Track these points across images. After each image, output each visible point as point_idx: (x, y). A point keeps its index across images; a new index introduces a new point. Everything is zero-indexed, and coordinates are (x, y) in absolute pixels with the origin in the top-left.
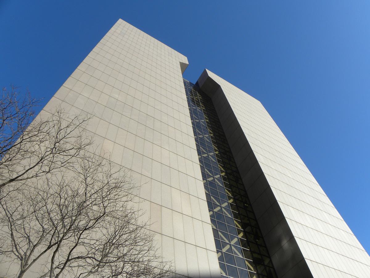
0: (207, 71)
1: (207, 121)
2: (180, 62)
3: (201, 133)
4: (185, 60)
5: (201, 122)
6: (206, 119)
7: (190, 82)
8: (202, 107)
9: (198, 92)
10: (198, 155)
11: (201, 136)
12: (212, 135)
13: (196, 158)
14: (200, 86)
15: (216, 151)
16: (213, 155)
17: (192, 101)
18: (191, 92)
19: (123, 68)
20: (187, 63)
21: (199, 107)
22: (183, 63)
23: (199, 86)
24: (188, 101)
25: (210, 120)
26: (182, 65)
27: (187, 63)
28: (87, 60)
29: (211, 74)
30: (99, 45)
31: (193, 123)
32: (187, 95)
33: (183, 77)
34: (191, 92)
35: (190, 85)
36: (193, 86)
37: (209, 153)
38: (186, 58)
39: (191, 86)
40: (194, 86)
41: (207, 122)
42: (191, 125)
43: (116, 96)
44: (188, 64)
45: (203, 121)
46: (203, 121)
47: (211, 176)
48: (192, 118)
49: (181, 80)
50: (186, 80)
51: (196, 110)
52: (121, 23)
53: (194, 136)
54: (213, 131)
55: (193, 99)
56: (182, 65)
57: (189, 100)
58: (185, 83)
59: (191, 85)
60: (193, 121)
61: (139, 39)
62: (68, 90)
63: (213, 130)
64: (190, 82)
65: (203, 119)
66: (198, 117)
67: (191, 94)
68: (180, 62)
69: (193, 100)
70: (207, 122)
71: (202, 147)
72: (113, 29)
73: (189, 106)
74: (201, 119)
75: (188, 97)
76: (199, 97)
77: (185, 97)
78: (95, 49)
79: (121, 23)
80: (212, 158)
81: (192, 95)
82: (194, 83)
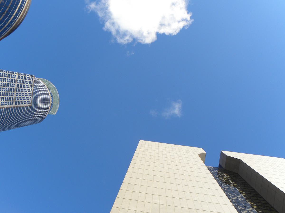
0: (223, 152)
1: (244, 194)
2: (198, 154)
3: (234, 195)
4: (201, 151)
5: (239, 198)
6: (242, 193)
7: (214, 167)
8: (227, 176)
9: (224, 172)
10: (229, 199)
11: (235, 198)
12: (255, 207)
13: (228, 201)
14: (224, 166)
15: (253, 205)
16: (252, 210)
17: (222, 183)
18: (218, 175)
19: (142, 186)
20: (204, 152)
21: (231, 185)
22: (201, 154)
23: (223, 168)
24: (219, 184)
25: (257, 206)
26: (201, 155)
27: (204, 152)
28: (126, 180)
29: (228, 154)
30: (131, 165)
31: (232, 202)
32: (215, 179)
33: (206, 165)
34: (218, 175)
35: (215, 169)
36: (218, 169)
37: (248, 209)
38: (202, 149)
39: (216, 170)
40: (218, 169)
41: (245, 196)
42: (231, 204)
43: (158, 201)
44: (205, 153)
45: (240, 196)
46: (241, 197)
47: (245, 210)
48: (229, 198)
49: (206, 167)
50: (209, 167)
51: (229, 188)
52: (141, 141)
53: (229, 199)
54: (243, 191)
55: (222, 180)
56: (201, 155)
57: (219, 182)
58: (209, 169)
59: (216, 169)
60: (231, 200)
61: (163, 148)
62: (118, 209)
63: (253, 202)
64: (214, 167)
65: (240, 195)
66: (234, 194)
67: (218, 176)
68: (198, 154)
69: (223, 181)
70: (245, 196)
71: (239, 206)
72: (137, 149)
73: (222, 188)
74: (238, 195)
75: (217, 180)
76: (227, 177)
77: (214, 181)
78: (130, 169)
79: (141, 141)
80: (240, 199)
81: (220, 177)
82: (218, 166)
